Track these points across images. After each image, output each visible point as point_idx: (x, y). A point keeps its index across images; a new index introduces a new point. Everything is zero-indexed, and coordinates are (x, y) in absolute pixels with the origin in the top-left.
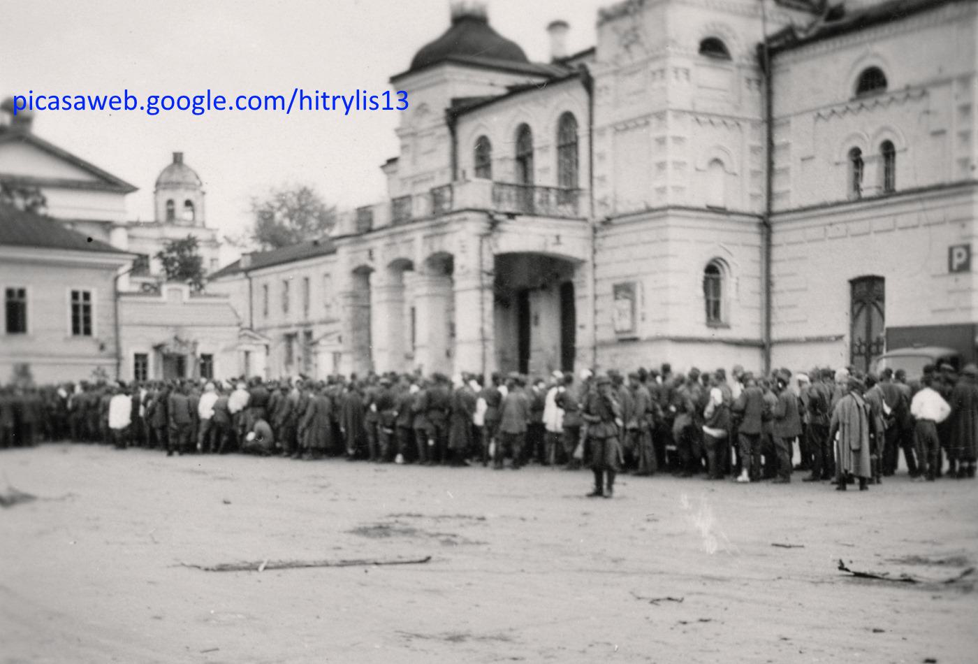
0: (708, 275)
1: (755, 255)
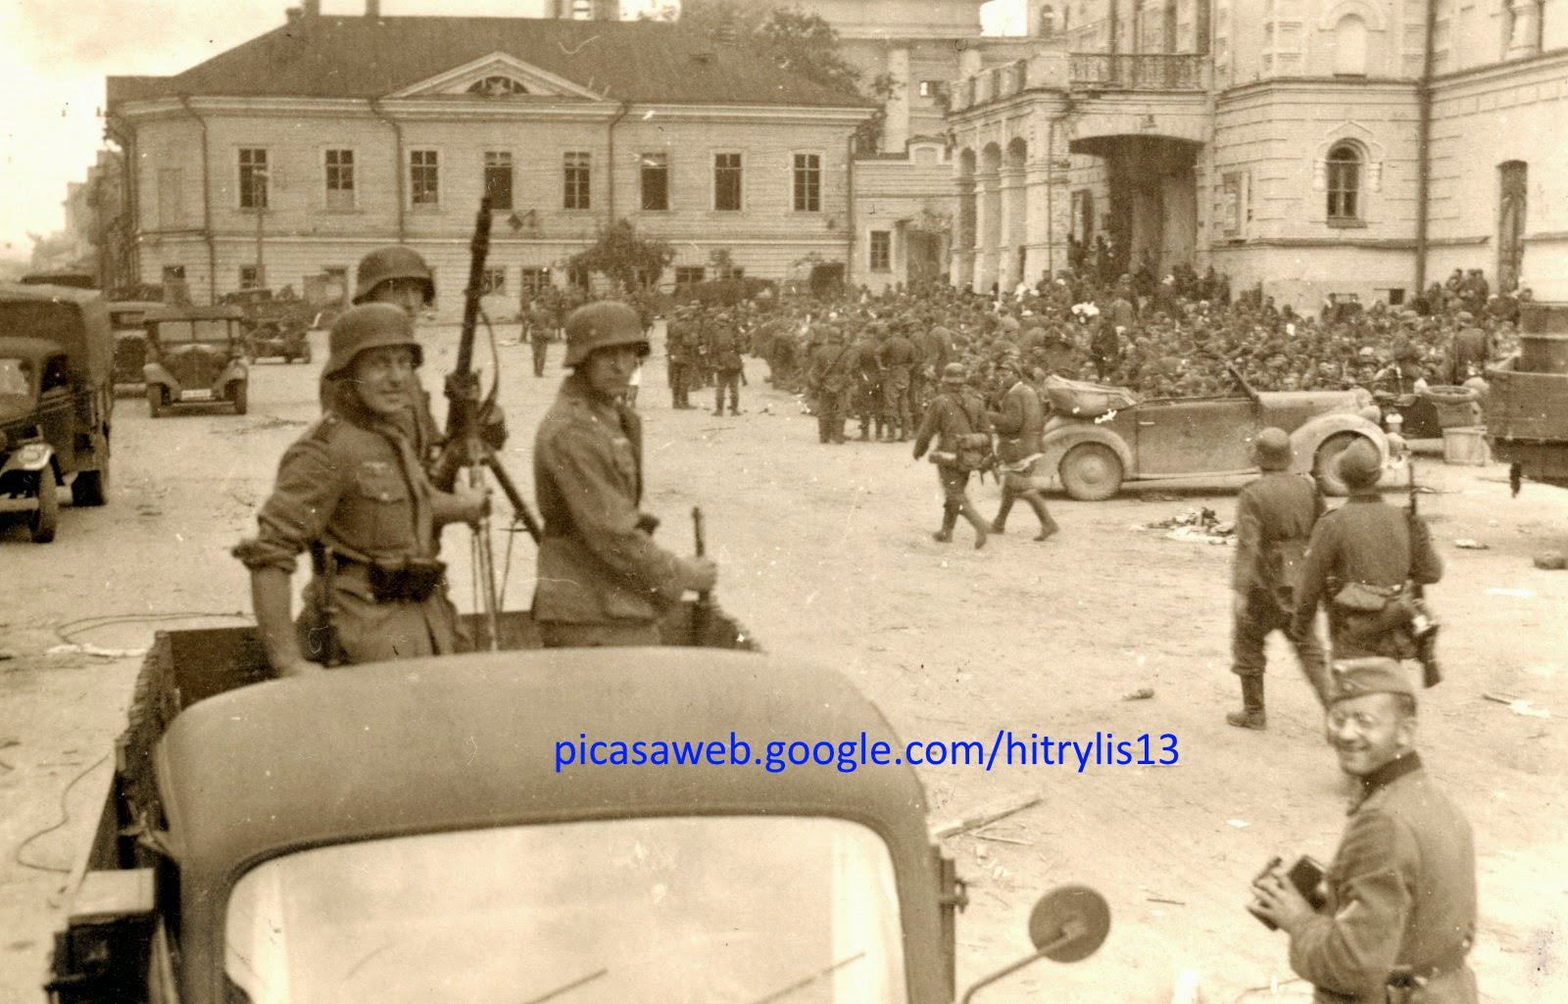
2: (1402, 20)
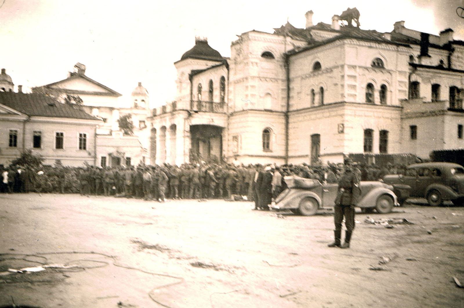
0: (265, 133)
1: (283, 126)
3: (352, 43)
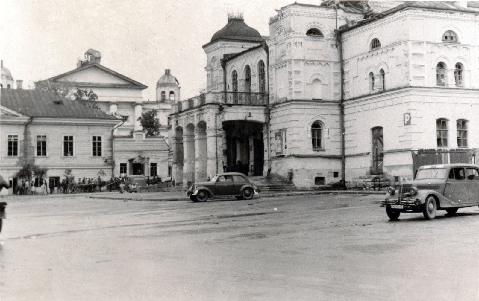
2: (333, 82)
3: (417, 14)
